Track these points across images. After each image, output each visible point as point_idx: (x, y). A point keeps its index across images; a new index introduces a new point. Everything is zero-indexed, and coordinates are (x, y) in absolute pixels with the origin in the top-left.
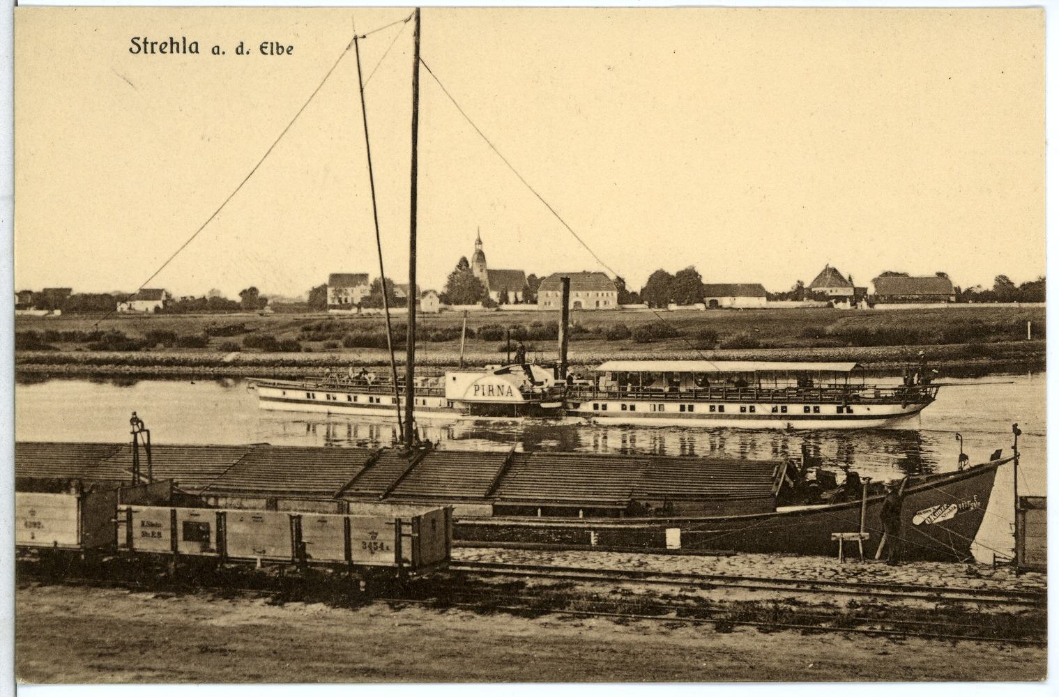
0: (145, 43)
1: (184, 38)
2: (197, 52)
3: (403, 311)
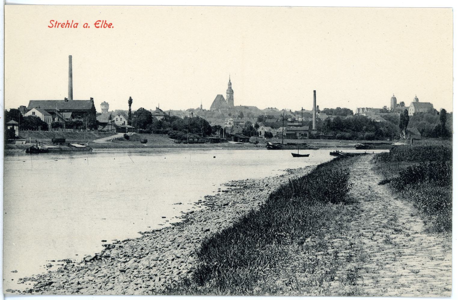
0: (56, 23)
3: (15, 127)
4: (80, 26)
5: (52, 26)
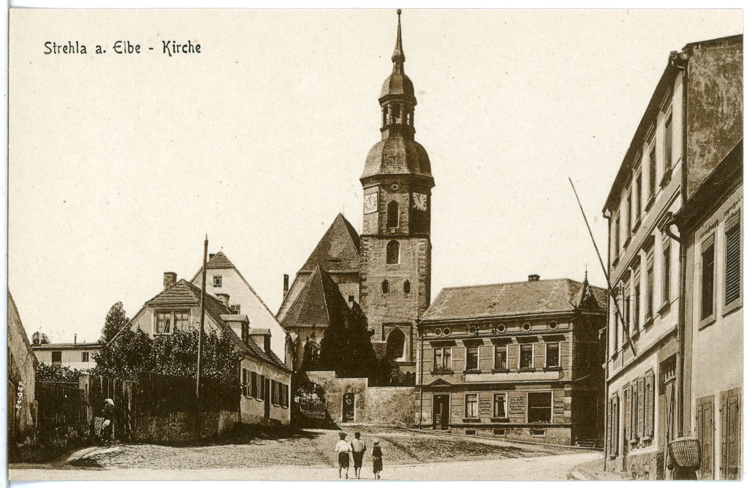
2: (85, 52)
5: (49, 51)
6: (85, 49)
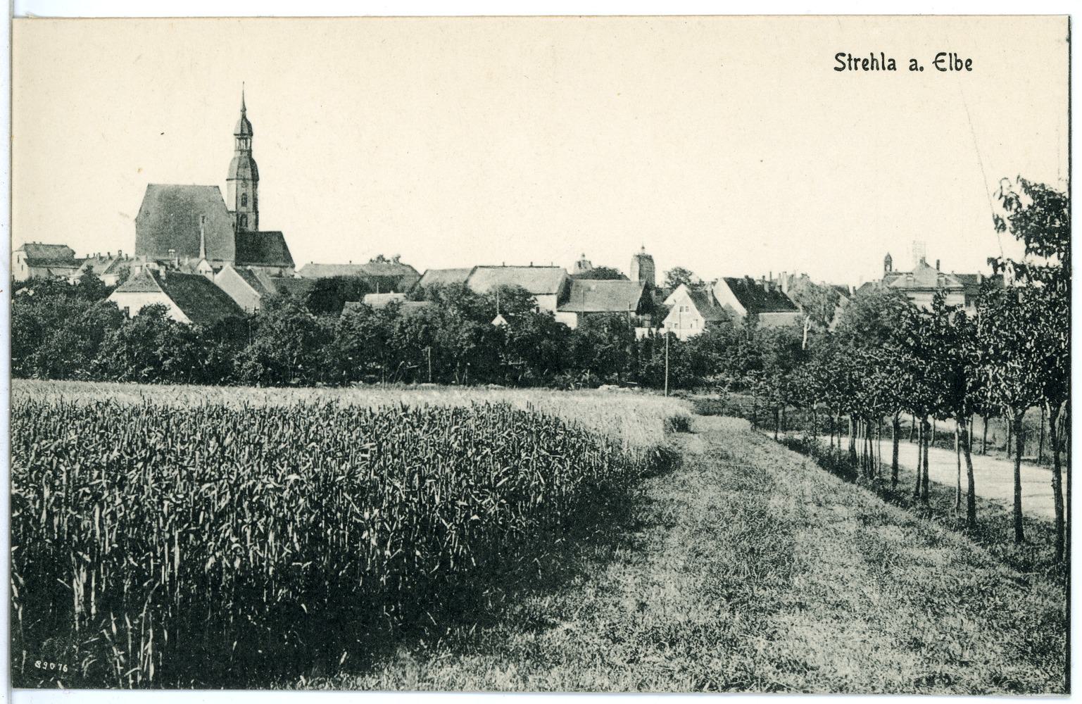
0: (850, 60)
1: (882, 54)
2: (895, 69)
4: (926, 61)
5: (841, 66)
6: (894, 64)
